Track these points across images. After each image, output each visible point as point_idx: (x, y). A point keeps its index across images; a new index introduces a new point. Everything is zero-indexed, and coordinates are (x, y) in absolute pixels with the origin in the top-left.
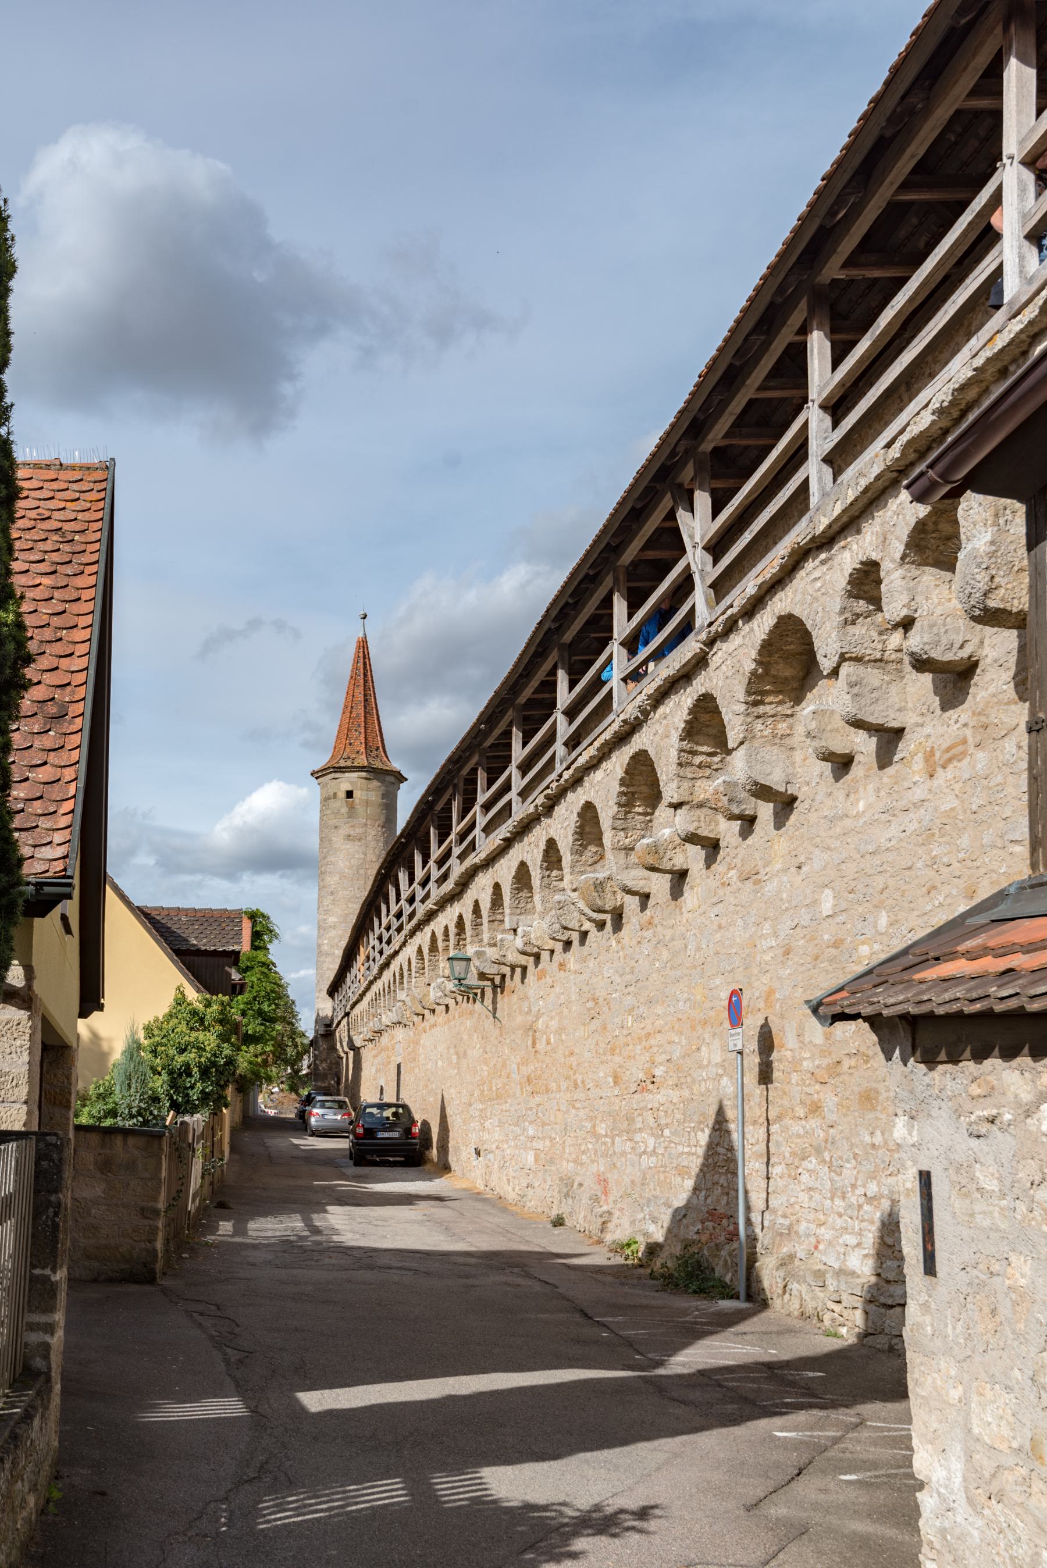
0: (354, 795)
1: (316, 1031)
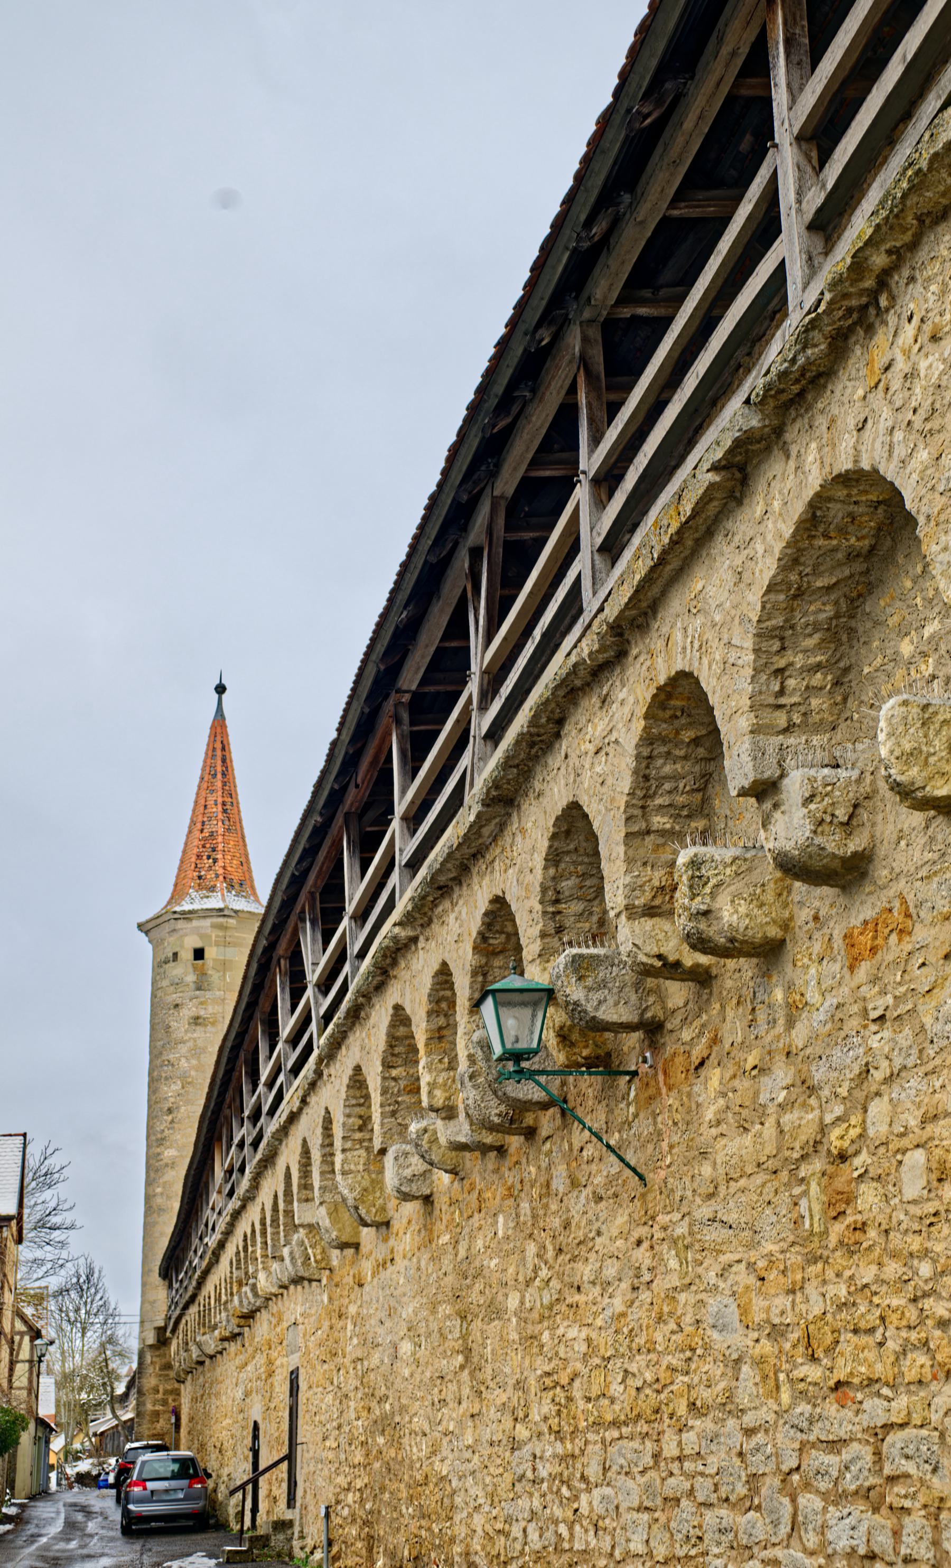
0: (206, 955)
1: (143, 1340)
